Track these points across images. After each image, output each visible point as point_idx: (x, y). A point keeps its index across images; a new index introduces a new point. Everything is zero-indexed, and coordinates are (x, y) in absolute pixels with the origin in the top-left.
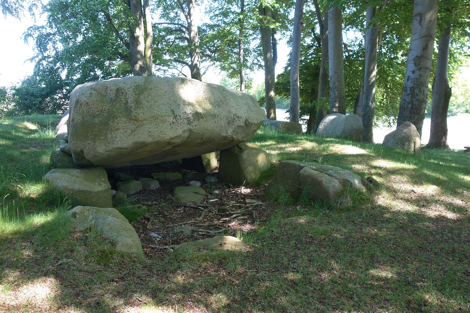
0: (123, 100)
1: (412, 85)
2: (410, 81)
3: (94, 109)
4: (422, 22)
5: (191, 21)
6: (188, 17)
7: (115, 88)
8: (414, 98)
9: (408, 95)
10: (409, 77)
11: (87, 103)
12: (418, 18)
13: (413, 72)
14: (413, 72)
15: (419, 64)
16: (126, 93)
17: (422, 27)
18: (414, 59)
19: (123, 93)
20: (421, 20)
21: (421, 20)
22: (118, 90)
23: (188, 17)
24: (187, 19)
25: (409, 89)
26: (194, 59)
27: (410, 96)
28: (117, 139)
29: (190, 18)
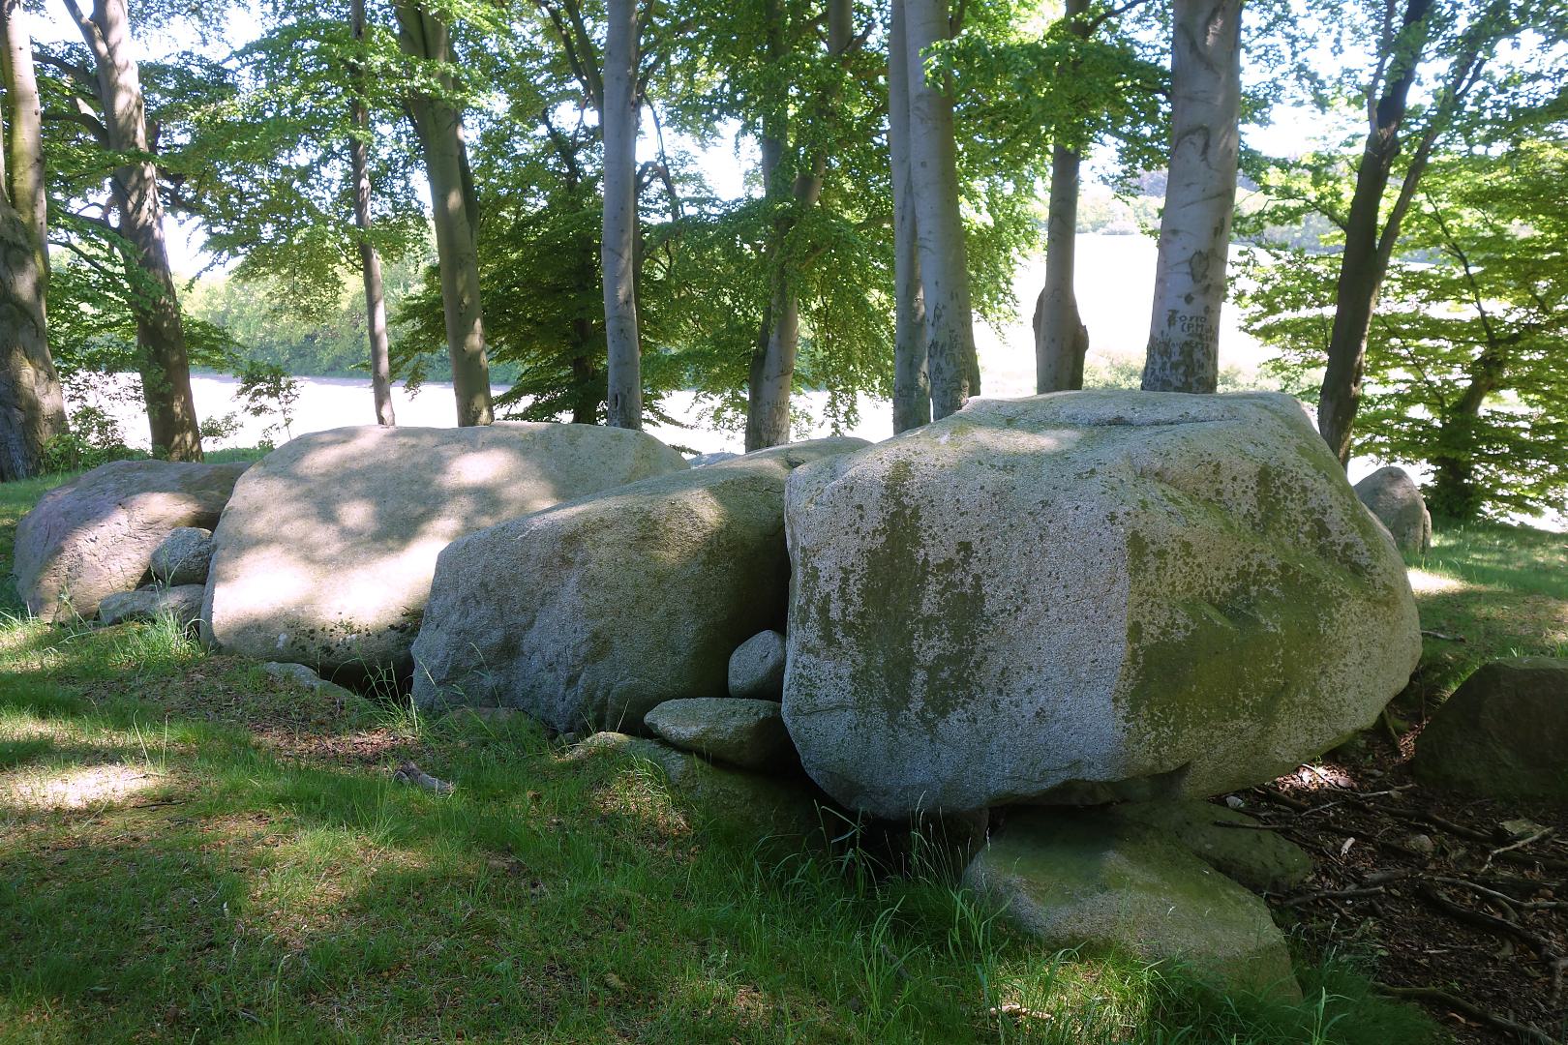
0: (1301, 519)
1: (1184, 337)
2: (1179, 324)
3: (1211, 571)
4: (1211, 151)
5: (111, 51)
6: (97, 31)
7: (1250, 468)
8: (1193, 374)
9: (1175, 366)
10: (1175, 312)
11: (1187, 545)
12: (1199, 141)
13: (1189, 299)
14: (1189, 299)
15: (1204, 276)
16: (1304, 489)
17: (1209, 166)
18: (1190, 262)
19: (1290, 490)
20: (1207, 146)
21: (1207, 146)
22: (1264, 476)
23: (97, 31)
24: (92, 42)
25: (1177, 350)
26: (139, 206)
27: (1181, 370)
28: (1350, 695)
29: (105, 39)
